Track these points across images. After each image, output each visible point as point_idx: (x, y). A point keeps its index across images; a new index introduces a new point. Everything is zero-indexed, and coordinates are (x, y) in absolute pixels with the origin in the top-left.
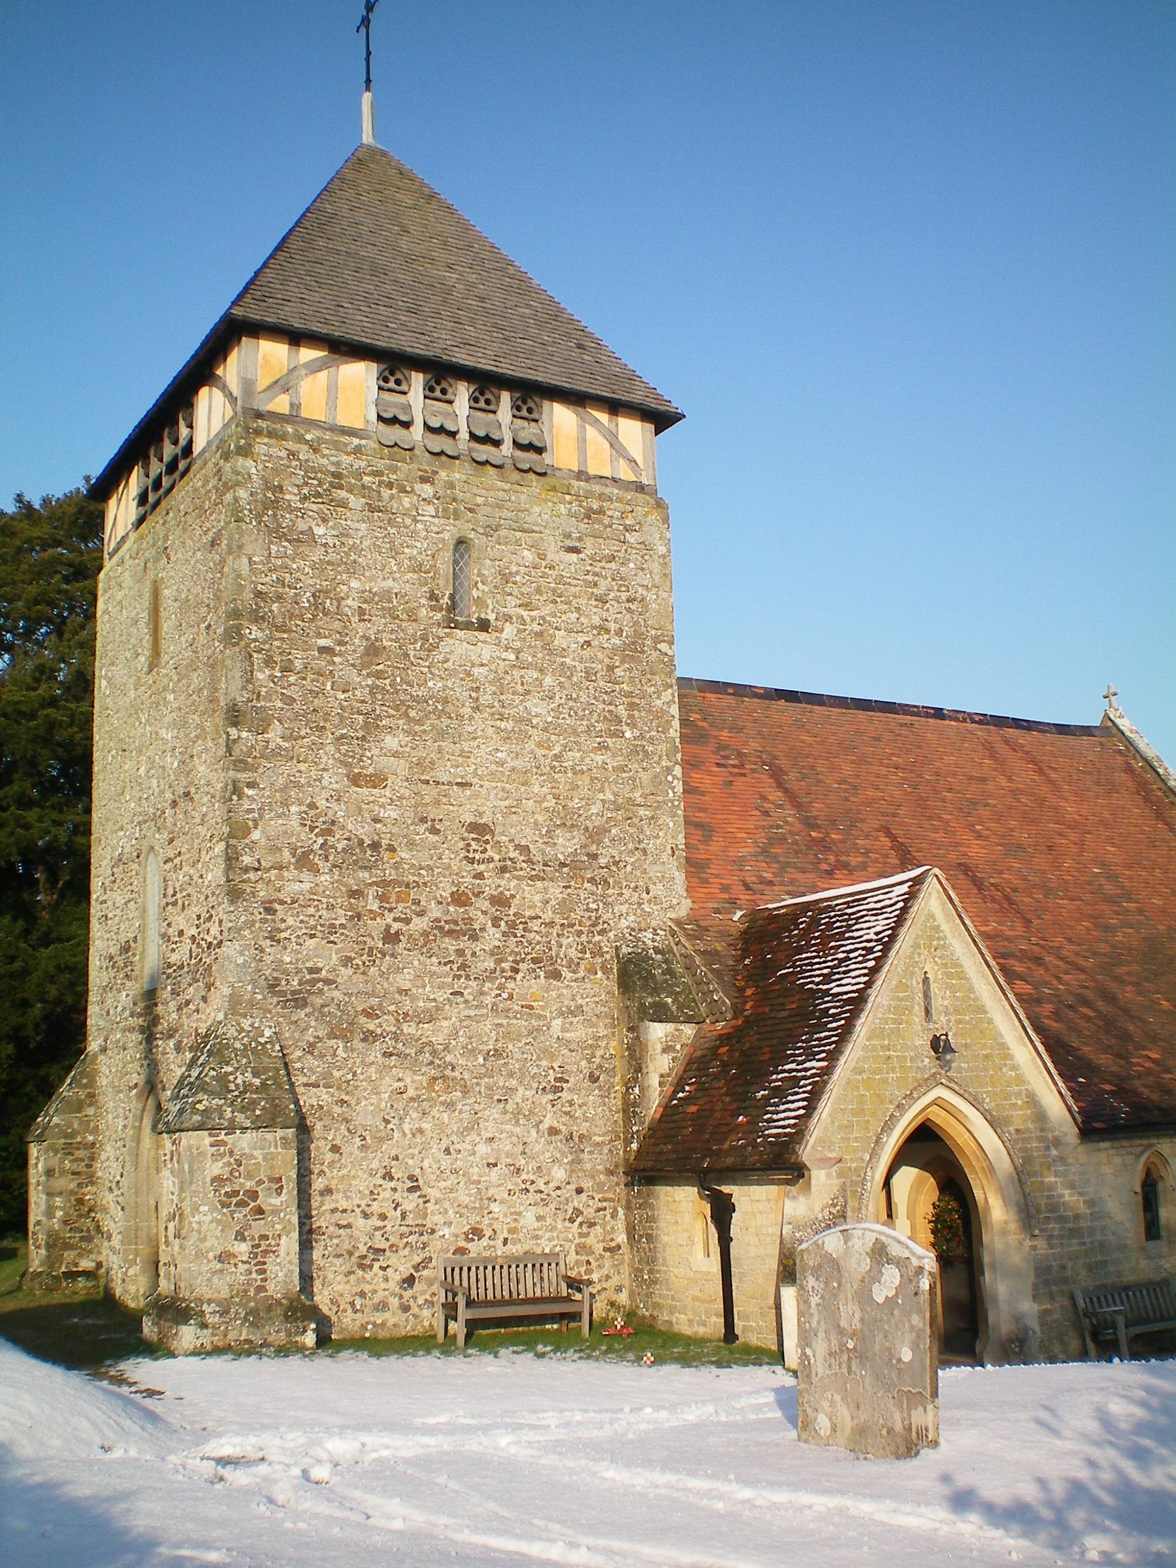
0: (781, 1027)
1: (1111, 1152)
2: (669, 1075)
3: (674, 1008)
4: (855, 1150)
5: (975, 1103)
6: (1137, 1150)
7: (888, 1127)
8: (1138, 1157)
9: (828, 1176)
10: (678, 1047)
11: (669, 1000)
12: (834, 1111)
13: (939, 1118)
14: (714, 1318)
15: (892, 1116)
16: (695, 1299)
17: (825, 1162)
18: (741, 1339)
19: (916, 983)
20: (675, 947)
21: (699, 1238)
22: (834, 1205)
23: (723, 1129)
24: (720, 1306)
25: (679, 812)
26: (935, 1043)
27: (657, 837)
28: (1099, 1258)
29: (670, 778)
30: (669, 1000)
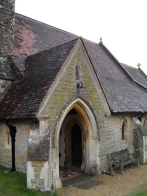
0: (34, 79)
1: (117, 118)
2: (3, 94)
3: (6, 76)
4: (54, 115)
5: (88, 104)
6: (121, 118)
7: (64, 108)
8: (122, 120)
9: (45, 123)
10: (6, 86)
11: (5, 74)
12: (48, 103)
13: (78, 107)
14: (10, 163)
15: (65, 105)
16: (5, 156)
17: (45, 118)
18: (17, 170)
19: (74, 67)
20: (9, 62)
21: (7, 139)
22: (46, 132)
23: (14, 107)
24: (11, 159)
25: (13, 30)
26: (78, 86)
27: (7, 34)
28: (113, 145)
29: (11, 21)
30: (5, 74)
